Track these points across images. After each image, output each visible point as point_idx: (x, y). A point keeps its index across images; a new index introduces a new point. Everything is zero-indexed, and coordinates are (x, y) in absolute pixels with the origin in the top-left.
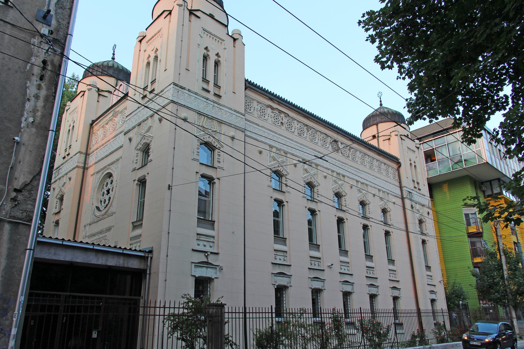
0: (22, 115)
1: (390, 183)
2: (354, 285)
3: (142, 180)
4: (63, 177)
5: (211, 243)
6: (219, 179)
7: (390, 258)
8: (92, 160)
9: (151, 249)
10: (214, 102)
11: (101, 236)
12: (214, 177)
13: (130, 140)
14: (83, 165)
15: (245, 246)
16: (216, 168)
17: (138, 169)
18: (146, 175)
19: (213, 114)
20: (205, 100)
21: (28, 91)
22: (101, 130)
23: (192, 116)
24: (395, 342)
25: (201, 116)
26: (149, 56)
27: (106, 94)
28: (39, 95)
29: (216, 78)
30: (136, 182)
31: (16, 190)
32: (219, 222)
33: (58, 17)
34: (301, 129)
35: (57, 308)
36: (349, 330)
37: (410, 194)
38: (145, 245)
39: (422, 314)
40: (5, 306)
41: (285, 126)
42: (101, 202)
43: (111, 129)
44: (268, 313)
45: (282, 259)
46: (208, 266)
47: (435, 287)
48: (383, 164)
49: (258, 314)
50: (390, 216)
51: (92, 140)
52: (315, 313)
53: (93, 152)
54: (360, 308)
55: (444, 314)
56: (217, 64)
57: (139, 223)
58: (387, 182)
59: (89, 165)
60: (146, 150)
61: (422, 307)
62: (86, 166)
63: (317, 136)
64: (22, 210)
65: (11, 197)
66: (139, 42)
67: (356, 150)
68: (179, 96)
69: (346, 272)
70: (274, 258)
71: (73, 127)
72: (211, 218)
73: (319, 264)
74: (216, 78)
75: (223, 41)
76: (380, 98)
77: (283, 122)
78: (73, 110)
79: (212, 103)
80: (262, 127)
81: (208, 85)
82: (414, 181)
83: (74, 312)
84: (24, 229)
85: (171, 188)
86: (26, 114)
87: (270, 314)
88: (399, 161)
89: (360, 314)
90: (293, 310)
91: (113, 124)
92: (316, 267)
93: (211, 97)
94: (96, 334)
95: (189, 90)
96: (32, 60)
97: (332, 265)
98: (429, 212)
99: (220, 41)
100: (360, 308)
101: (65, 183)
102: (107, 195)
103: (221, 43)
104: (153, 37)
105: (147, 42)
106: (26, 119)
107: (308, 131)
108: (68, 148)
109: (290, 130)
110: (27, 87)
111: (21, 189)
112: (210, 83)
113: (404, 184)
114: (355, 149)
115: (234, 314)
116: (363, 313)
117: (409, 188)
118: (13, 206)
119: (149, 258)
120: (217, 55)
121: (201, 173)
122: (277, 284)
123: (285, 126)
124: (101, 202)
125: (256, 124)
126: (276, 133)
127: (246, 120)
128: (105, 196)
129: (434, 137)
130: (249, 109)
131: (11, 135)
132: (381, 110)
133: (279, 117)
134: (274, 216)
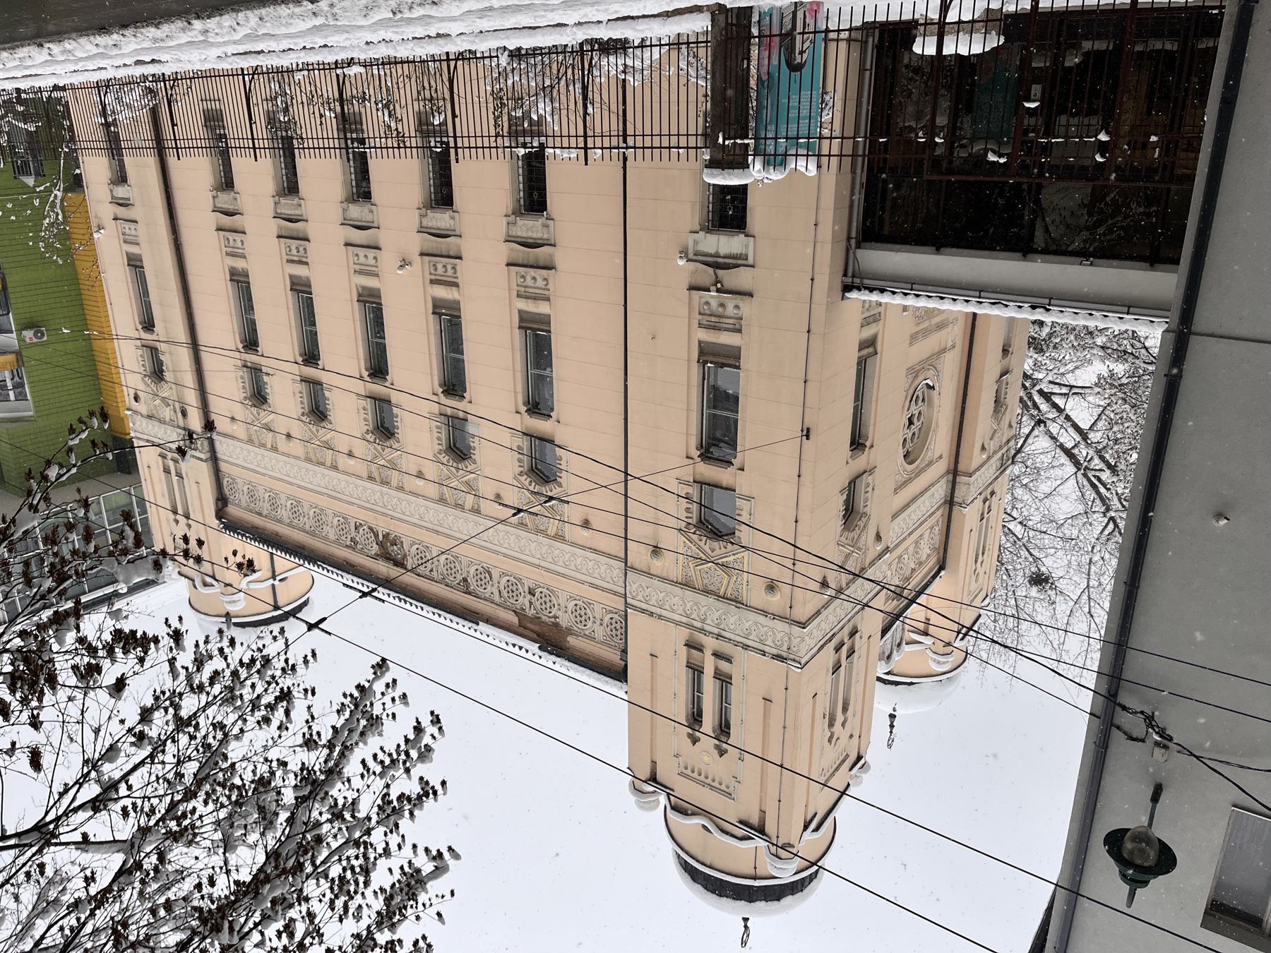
1: (243, 467)
2: (341, 220)
4: (995, 452)
5: (708, 312)
8: (940, 491)
10: (702, 630)
13: (878, 537)
14: (959, 479)
16: (694, 481)
17: (865, 472)
18: (850, 460)
19: (703, 604)
22: (924, 558)
23: (757, 595)
25: (733, 597)
26: (843, 725)
29: (696, 686)
30: (868, 444)
32: (689, 360)
36: (351, 111)
41: (523, 587)
42: (923, 400)
43: (906, 562)
45: (529, 278)
46: (715, 259)
47: (115, 214)
48: (265, 512)
51: (941, 534)
53: (938, 509)
56: (695, 718)
58: (254, 471)
59: (944, 480)
60: (851, 512)
61: (151, 161)
62: (951, 476)
63: (442, 569)
66: (862, 753)
67: (337, 542)
68: (786, 639)
69: (361, 252)
70: (550, 282)
71: (976, 562)
73: (432, 268)
74: (696, 686)
77: (529, 597)
79: (707, 628)
80: (583, 583)
81: (716, 669)
85: (805, 433)
87: (460, 144)
90: (501, 155)
91: (902, 572)
93: (710, 643)
95: (764, 653)
98: (136, 401)
99: (688, 772)
101: (991, 439)
103: (686, 768)
104: (837, 769)
105: (847, 756)
107: (465, 580)
108: (986, 516)
109: (511, 579)
112: (712, 673)
114: (340, 544)
115: (656, 144)
120: (695, 741)
121: (731, 469)
123: (523, 587)
124: (923, 400)
125: (597, 587)
126: (548, 570)
130: (614, 621)
133: (539, 607)
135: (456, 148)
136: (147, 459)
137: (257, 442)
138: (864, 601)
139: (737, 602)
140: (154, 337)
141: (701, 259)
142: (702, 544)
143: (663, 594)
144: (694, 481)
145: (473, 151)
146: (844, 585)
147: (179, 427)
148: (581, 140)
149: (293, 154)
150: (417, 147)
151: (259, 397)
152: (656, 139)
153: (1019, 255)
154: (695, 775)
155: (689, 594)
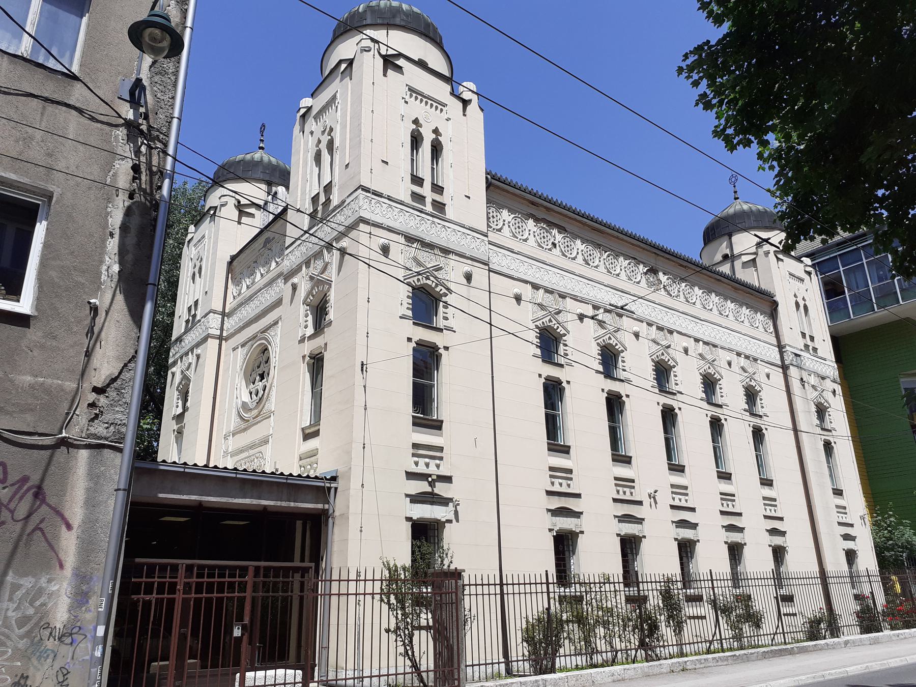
0: (102, 262)
3: (317, 355)
6: (446, 348)
7: (764, 476)
9: (334, 475)
11: (251, 452)
12: (440, 345)
15: (496, 461)
20: (418, 214)
21: (110, 220)
23: (690, 343)
24: (778, 632)
26: (319, 141)
27: (252, 210)
28: (128, 224)
30: (307, 359)
31: (97, 390)
33: (155, 88)
34: (589, 252)
35: (173, 588)
37: (798, 358)
38: (323, 468)
39: (831, 580)
40: (84, 588)
44: (541, 583)
49: (522, 587)
50: (761, 400)
52: (630, 576)
54: (710, 570)
55: (872, 579)
57: (313, 430)
61: (830, 568)
64: (106, 423)
65: (88, 402)
69: (683, 504)
72: (436, 415)
75: (444, 105)
76: (735, 186)
78: (199, 241)
82: (804, 335)
83: (202, 594)
84: (112, 455)
86: (107, 259)
87: (544, 586)
88: (775, 298)
89: (710, 582)
92: (628, 497)
94: (240, 630)
96: (114, 166)
97: (656, 492)
99: (440, 107)
100: (710, 570)
102: (261, 381)
103: (442, 110)
106: (108, 267)
110: (108, 214)
111: (104, 387)
113: (786, 339)
116: (717, 580)
117: (794, 348)
118: (92, 416)
119: (333, 491)
122: (556, 529)
127: (490, 243)
128: (256, 383)
129: (838, 251)
130: (495, 223)
131: (84, 297)
132: (737, 207)
134: (546, 408)
135: (548, 583)
136: (826, 348)
137: (751, 359)
138: (307, 235)
139: (410, 239)
140: (823, 437)
141: (444, 502)
142: (668, 357)
143: (462, 244)
144: (442, 329)
145: (485, 582)
146: (325, 251)
147: (805, 370)
148: (715, 585)
149: (625, 577)
150: (697, 581)
151: (751, 395)
152: (480, 592)
153: (269, 509)
154: (435, 104)
155: (443, 243)
